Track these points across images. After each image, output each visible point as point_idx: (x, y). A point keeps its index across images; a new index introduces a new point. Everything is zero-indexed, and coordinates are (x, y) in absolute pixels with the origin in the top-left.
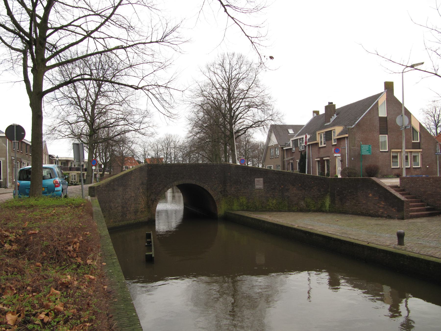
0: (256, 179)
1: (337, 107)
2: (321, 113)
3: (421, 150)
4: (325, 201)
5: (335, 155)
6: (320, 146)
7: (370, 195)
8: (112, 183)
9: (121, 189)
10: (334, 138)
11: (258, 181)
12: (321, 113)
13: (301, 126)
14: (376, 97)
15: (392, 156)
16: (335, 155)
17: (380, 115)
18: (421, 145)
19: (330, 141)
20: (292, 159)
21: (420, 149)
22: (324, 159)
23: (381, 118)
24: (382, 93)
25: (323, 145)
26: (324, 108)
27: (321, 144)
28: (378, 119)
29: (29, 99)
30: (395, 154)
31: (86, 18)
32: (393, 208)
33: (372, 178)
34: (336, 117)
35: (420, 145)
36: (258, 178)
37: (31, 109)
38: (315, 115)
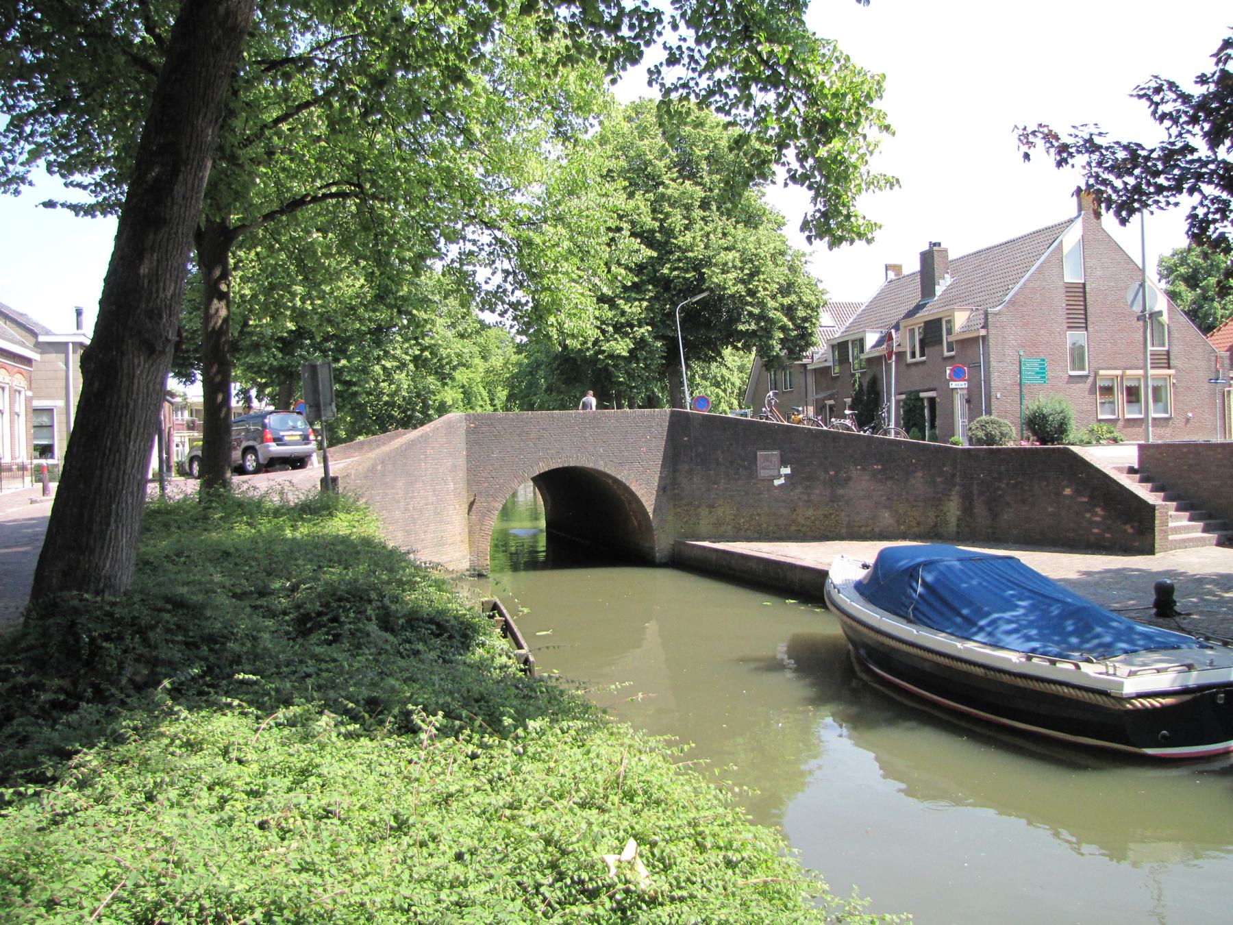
4: (945, 509)
5: (953, 385)
6: (909, 360)
7: (1068, 491)
10: (951, 339)
11: (766, 459)
14: (1052, 234)
16: (953, 385)
17: (1068, 279)
19: (937, 348)
21: (1169, 368)
22: (922, 395)
23: (1069, 287)
24: (1071, 221)
25: (918, 358)
27: (913, 355)
32: (1125, 523)
33: (650, 510)
34: (949, 283)
35: (1169, 359)
36: (764, 449)
37: (112, 249)
38: (891, 275)
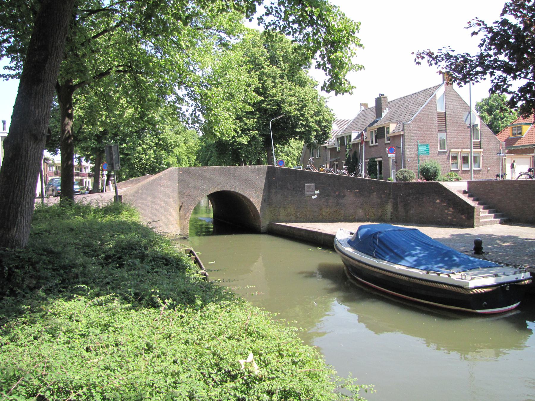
0: (306, 185)
1: (389, 100)
2: (369, 106)
3: (481, 150)
4: (386, 209)
5: (389, 155)
6: (371, 145)
7: (438, 201)
8: (140, 191)
9: (149, 198)
10: (388, 135)
11: (309, 187)
12: (369, 106)
13: (346, 121)
14: (432, 91)
15: (474, 170)
16: (389, 155)
17: (439, 110)
18: (482, 144)
19: (382, 140)
20: (337, 160)
21: (480, 148)
23: (439, 114)
25: (374, 144)
26: (375, 100)
27: (372, 142)
28: (436, 115)
29: (17, 93)
30: (454, 155)
31: (512, 178)
36: (308, 183)
38: (363, 108)
